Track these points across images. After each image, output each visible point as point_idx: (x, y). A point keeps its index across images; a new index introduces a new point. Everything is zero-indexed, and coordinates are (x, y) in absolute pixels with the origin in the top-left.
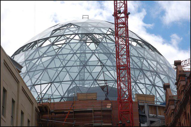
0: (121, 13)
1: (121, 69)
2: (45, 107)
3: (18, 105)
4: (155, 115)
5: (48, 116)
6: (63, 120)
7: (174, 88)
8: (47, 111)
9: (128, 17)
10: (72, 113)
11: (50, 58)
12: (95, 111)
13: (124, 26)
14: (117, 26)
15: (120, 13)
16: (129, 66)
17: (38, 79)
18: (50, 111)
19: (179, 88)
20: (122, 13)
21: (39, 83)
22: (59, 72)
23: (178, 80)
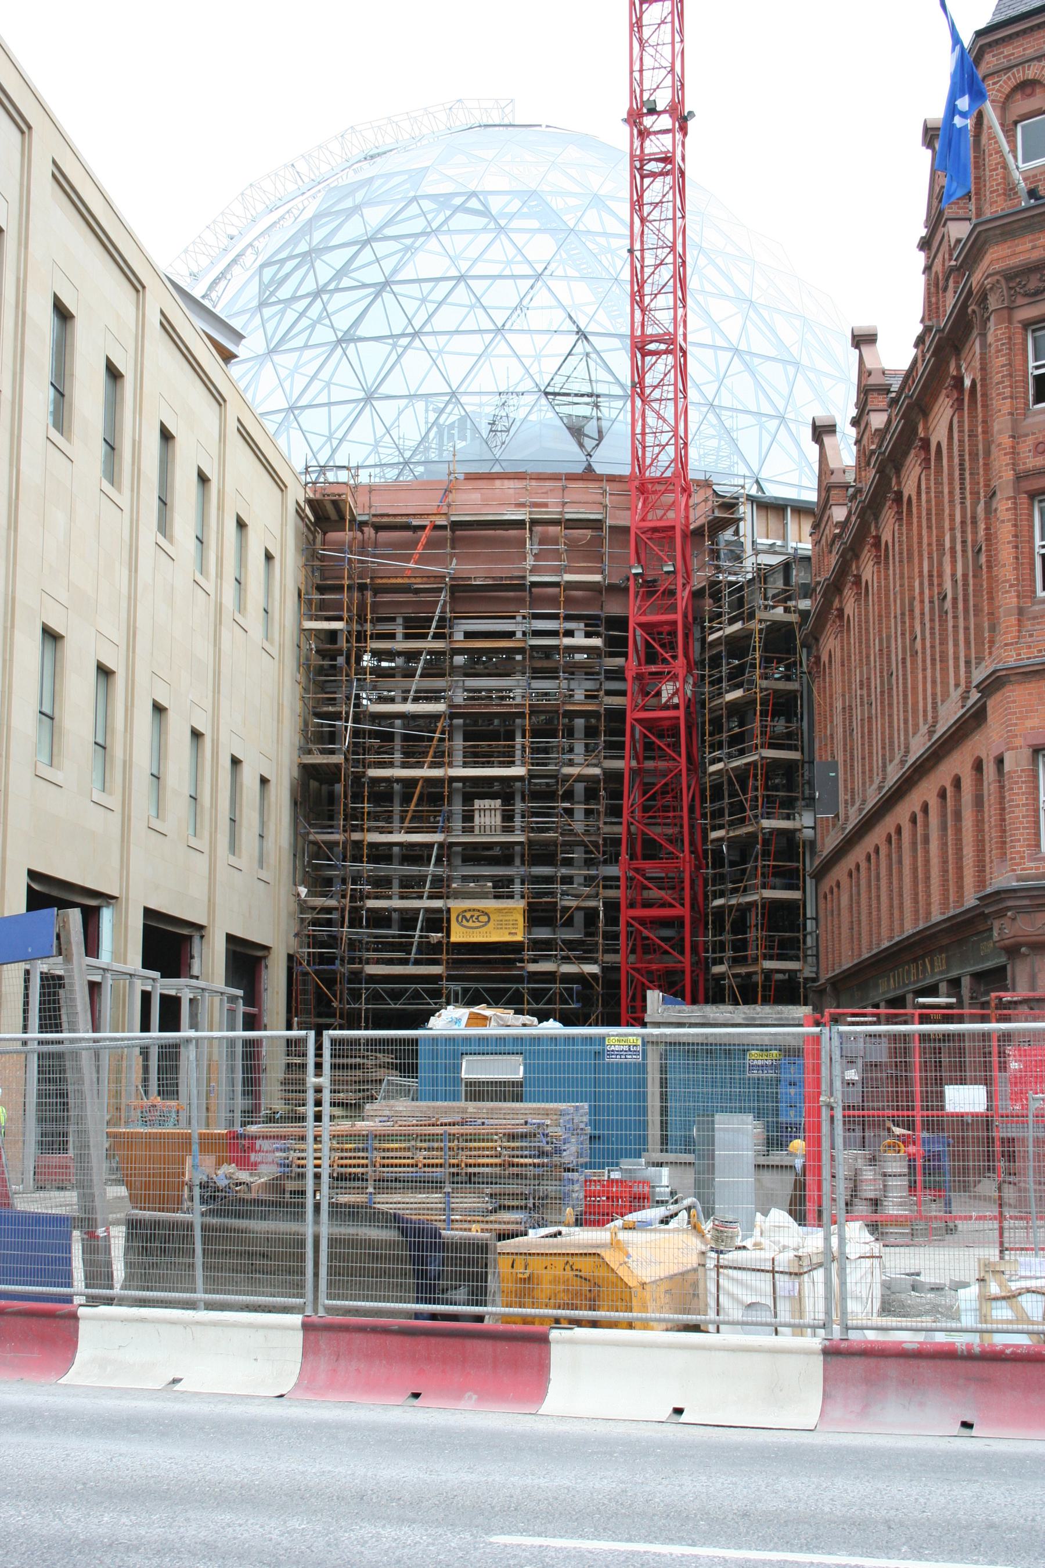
0: (659, 113)
1: (652, 353)
2: (335, 503)
3: (221, 493)
4: (779, 543)
5: (346, 536)
6: (407, 558)
7: (847, 433)
8: (342, 518)
9: (684, 130)
10: (443, 528)
11: (372, 290)
12: (534, 522)
13: (669, 167)
14: (641, 168)
15: (652, 111)
16: (685, 339)
17: (313, 378)
18: (353, 520)
19: (865, 441)
20: (665, 111)
21: (323, 399)
22: (400, 350)
23: (863, 407)
